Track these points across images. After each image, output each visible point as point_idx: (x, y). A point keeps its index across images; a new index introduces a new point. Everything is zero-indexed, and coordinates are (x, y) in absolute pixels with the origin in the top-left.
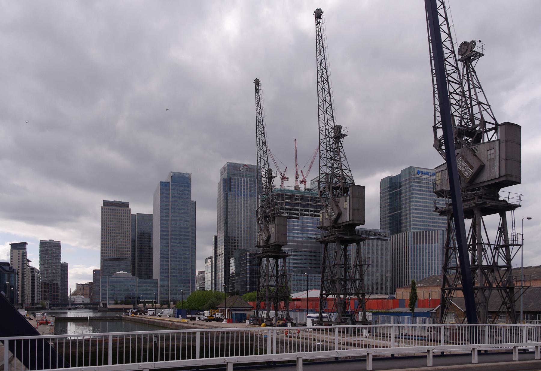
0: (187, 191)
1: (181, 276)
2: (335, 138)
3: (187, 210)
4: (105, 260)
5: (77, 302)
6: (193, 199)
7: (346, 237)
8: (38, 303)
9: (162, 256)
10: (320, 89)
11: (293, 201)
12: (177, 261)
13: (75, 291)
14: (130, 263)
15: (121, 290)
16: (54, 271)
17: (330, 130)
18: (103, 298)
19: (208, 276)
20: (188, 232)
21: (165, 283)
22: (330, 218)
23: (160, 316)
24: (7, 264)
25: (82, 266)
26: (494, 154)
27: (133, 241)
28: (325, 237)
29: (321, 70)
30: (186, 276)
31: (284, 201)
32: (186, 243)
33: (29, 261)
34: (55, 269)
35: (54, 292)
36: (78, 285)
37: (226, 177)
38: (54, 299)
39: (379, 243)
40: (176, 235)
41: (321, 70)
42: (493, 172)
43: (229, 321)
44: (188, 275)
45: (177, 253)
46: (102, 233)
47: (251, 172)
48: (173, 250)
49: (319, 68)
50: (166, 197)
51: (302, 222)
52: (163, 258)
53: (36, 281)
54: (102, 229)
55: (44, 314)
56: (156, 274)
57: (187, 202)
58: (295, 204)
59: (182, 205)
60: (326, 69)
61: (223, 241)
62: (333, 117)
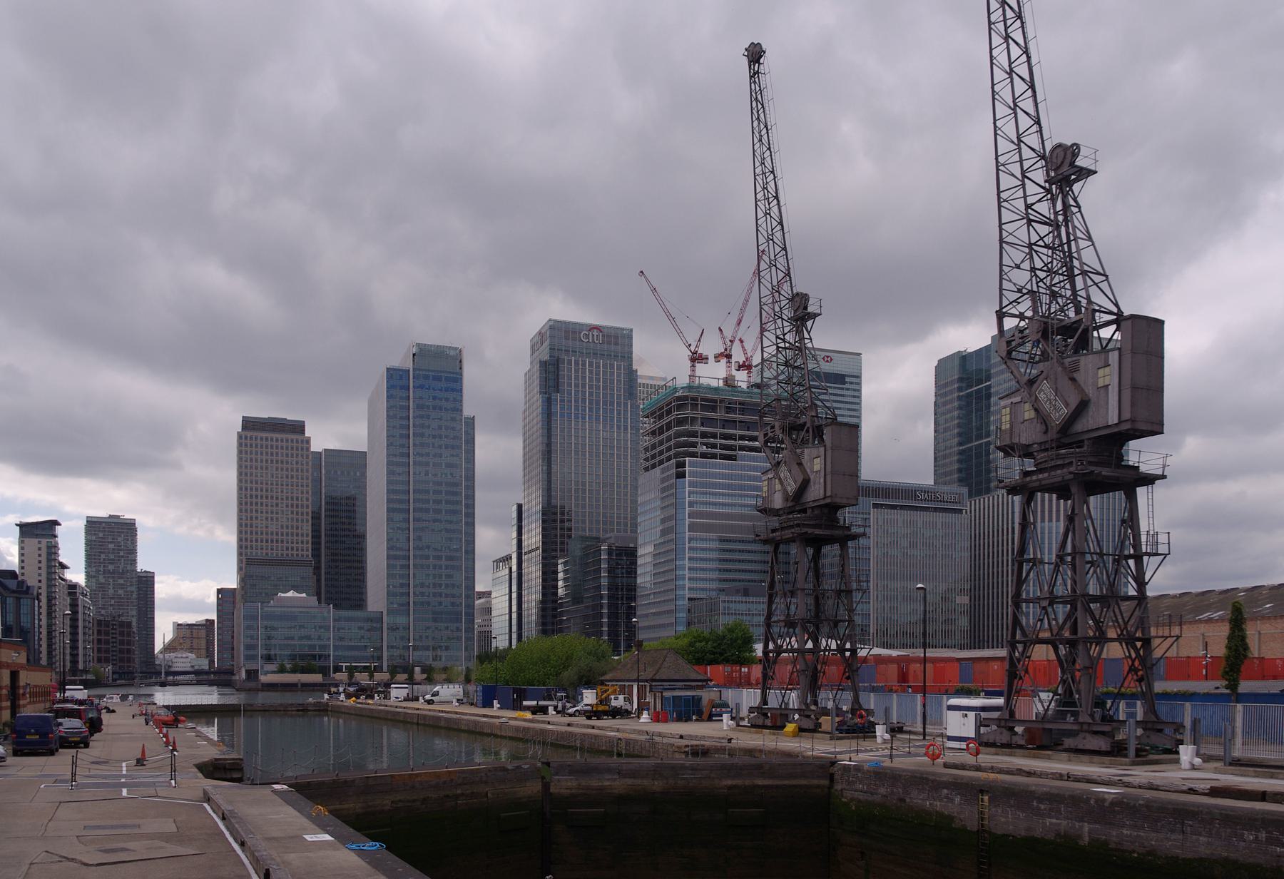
0: (453, 390)
1: (440, 604)
2: (796, 320)
3: (455, 438)
4: (249, 562)
5: (178, 666)
6: (467, 411)
7: (817, 532)
8: (85, 671)
9: (392, 553)
10: (760, 214)
11: (720, 414)
12: (428, 567)
13: (172, 641)
14: (311, 570)
15: (293, 638)
16: (121, 592)
17: (783, 304)
18: (247, 658)
19: (500, 604)
20: (455, 494)
21: (401, 620)
22: (785, 491)
23: (430, 702)
24: (12, 574)
25: (190, 578)
26: (1109, 376)
27: (316, 517)
28: (774, 531)
29: (764, 173)
30: (453, 604)
31: (699, 414)
32: (451, 522)
33: (63, 567)
34: (122, 586)
35: (122, 643)
36: (179, 627)
37: (547, 358)
38: (121, 660)
39: (940, 518)
40: (428, 501)
41: (764, 173)
42: (1109, 413)
43: (656, 718)
44: (462, 607)
45: (428, 547)
46: (239, 497)
47: (609, 343)
48: (420, 538)
49: (758, 171)
50: (402, 407)
51: (743, 468)
52: (396, 558)
53: (80, 616)
54: (240, 489)
55: (127, 696)
57: (453, 419)
58: (726, 423)
59: (440, 428)
60: (772, 172)
61: (539, 516)
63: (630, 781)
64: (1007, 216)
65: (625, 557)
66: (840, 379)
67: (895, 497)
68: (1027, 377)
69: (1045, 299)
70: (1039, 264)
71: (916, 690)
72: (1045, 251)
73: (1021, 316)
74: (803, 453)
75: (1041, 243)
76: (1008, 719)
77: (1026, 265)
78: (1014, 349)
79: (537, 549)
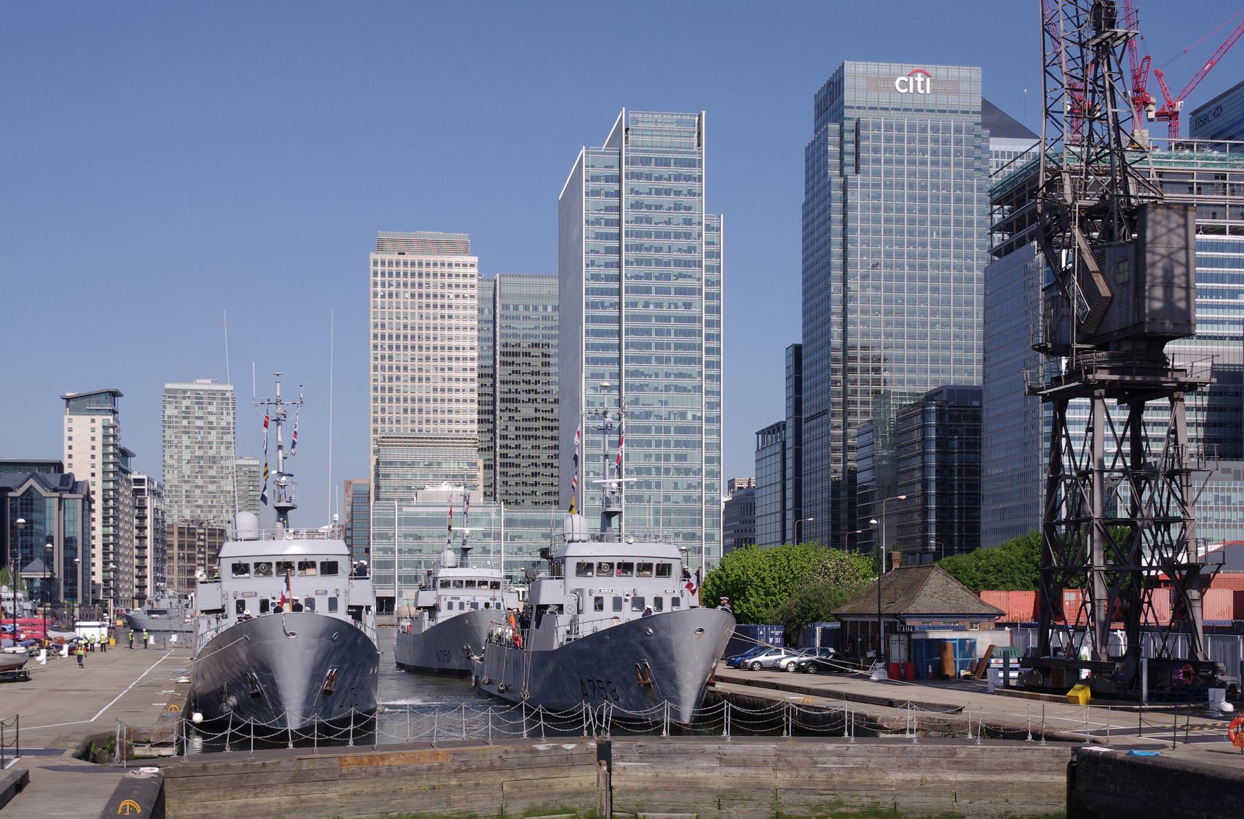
63: (735, 771)
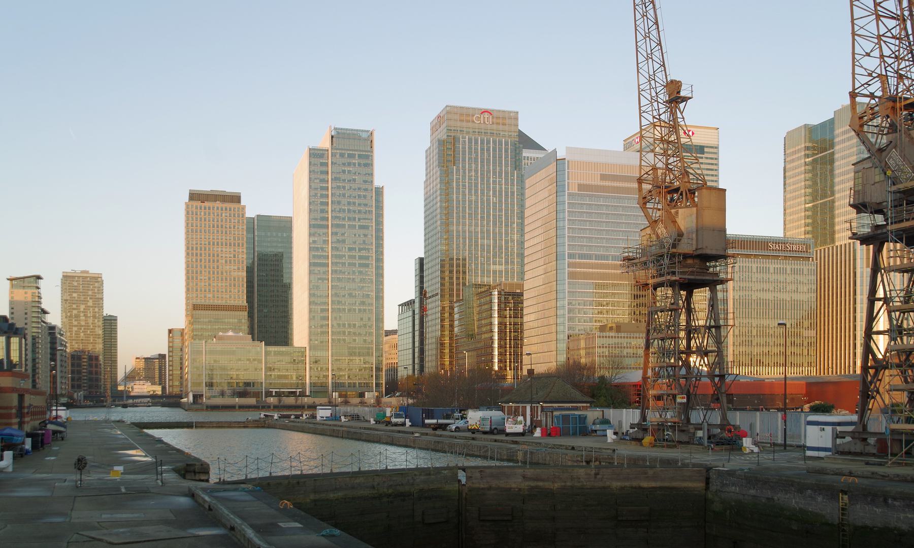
10: (638, 16)
14: (246, 313)
19: (405, 341)
24: (4, 318)
27: (250, 270)
33: (44, 312)
56: (300, 333)
62: (664, 65)
64: (858, 13)
65: (513, 300)
66: (701, 149)
67: (758, 247)
68: (877, 146)
69: (893, 81)
70: (886, 52)
71: (779, 410)
72: (893, 41)
73: (872, 96)
74: (677, 213)
75: (889, 34)
76: (861, 432)
77: (876, 53)
78: (866, 123)
79: (437, 294)
